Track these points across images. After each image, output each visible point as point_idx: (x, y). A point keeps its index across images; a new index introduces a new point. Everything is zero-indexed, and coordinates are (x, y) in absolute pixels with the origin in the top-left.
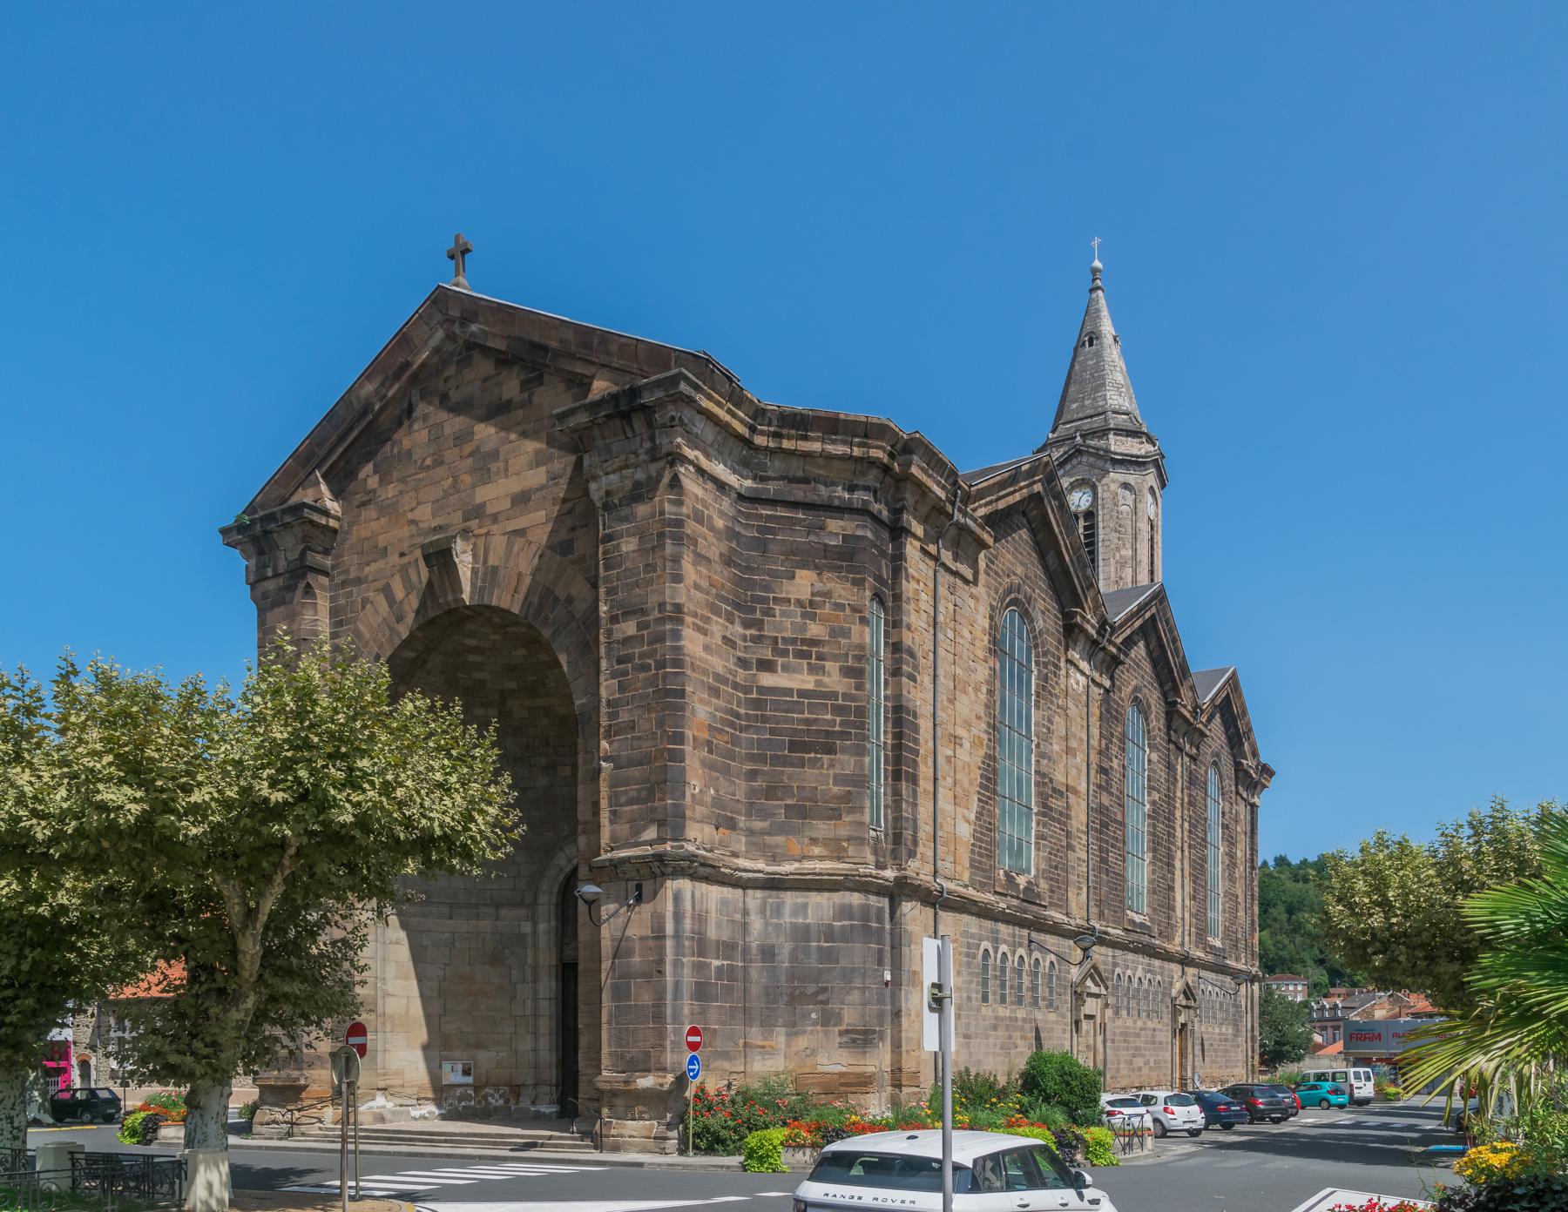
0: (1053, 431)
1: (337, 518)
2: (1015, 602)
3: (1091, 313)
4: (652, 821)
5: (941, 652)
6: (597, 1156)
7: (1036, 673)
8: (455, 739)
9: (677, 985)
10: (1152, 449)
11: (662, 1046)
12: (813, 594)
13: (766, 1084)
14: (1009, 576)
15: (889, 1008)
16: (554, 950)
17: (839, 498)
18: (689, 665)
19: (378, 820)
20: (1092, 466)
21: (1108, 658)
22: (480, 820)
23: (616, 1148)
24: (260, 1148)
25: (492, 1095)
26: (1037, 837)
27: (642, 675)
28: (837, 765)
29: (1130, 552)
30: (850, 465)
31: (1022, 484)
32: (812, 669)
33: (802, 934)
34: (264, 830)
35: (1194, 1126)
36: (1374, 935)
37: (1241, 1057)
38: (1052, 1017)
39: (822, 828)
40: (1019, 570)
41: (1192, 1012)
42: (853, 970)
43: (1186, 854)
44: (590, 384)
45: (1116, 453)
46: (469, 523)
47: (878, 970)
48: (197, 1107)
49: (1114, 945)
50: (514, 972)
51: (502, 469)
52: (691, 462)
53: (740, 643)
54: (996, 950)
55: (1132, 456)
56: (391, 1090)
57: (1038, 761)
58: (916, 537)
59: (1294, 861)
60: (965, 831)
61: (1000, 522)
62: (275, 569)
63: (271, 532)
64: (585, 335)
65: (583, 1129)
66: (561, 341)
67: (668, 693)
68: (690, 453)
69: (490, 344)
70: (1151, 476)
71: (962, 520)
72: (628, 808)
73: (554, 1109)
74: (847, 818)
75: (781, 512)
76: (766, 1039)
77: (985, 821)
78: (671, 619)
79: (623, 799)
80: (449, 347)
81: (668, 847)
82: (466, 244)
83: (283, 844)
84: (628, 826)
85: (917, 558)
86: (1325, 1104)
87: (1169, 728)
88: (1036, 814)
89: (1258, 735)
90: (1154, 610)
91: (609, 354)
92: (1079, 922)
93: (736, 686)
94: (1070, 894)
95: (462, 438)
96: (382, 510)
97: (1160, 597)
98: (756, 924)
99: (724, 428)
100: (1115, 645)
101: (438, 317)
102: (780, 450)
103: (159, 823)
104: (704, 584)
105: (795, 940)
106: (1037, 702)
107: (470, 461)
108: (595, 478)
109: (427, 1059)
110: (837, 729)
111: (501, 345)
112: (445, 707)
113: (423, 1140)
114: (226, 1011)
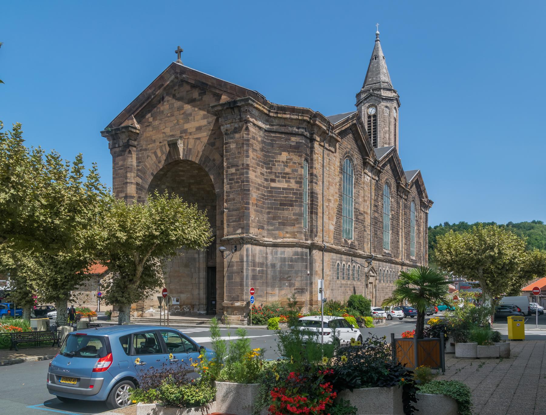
1: (139, 130)
2: (348, 156)
3: (376, 49)
4: (240, 227)
5: (325, 174)
6: (225, 326)
7: (354, 177)
9: (247, 275)
10: (395, 94)
11: (243, 294)
12: (287, 159)
13: (273, 305)
15: (309, 282)
16: (205, 263)
17: (295, 131)
20: (375, 100)
22: (203, 236)
23: (228, 324)
25: (185, 308)
26: (354, 228)
27: (237, 185)
29: (388, 129)
30: (298, 121)
32: (287, 182)
33: (283, 260)
35: (401, 317)
38: (359, 283)
39: (289, 229)
40: (349, 147)
42: (298, 270)
43: (403, 230)
46: (182, 135)
48: (123, 311)
49: (379, 260)
50: (192, 270)
52: (252, 122)
53: (265, 174)
54: (341, 263)
56: (154, 306)
58: (317, 141)
59: (451, 224)
60: (332, 228)
61: (343, 134)
62: (119, 145)
63: (118, 134)
64: (220, 83)
66: (212, 83)
67: (245, 190)
68: (251, 120)
70: (395, 104)
71: (331, 135)
72: (232, 223)
73: (205, 312)
74: (297, 226)
75: (278, 135)
78: (246, 168)
79: (231, 221)
80: (176, 80)
81: (245, 235)
84: (232, 229)
87: (398, 191)
89: (428, 191)
92: (368, 254)
93: (264, 187)
95: (180, 108)
96: (154, 128)
97: (394, 150)
98: (270, 257)
101: (173, 71)
102: (278, 117)
103: (130, 241)
104: (255, 157)
106: (355, 186)
107: (182, 116)
108: (222, 125)
110: (294, 199)
111: (193, 82)
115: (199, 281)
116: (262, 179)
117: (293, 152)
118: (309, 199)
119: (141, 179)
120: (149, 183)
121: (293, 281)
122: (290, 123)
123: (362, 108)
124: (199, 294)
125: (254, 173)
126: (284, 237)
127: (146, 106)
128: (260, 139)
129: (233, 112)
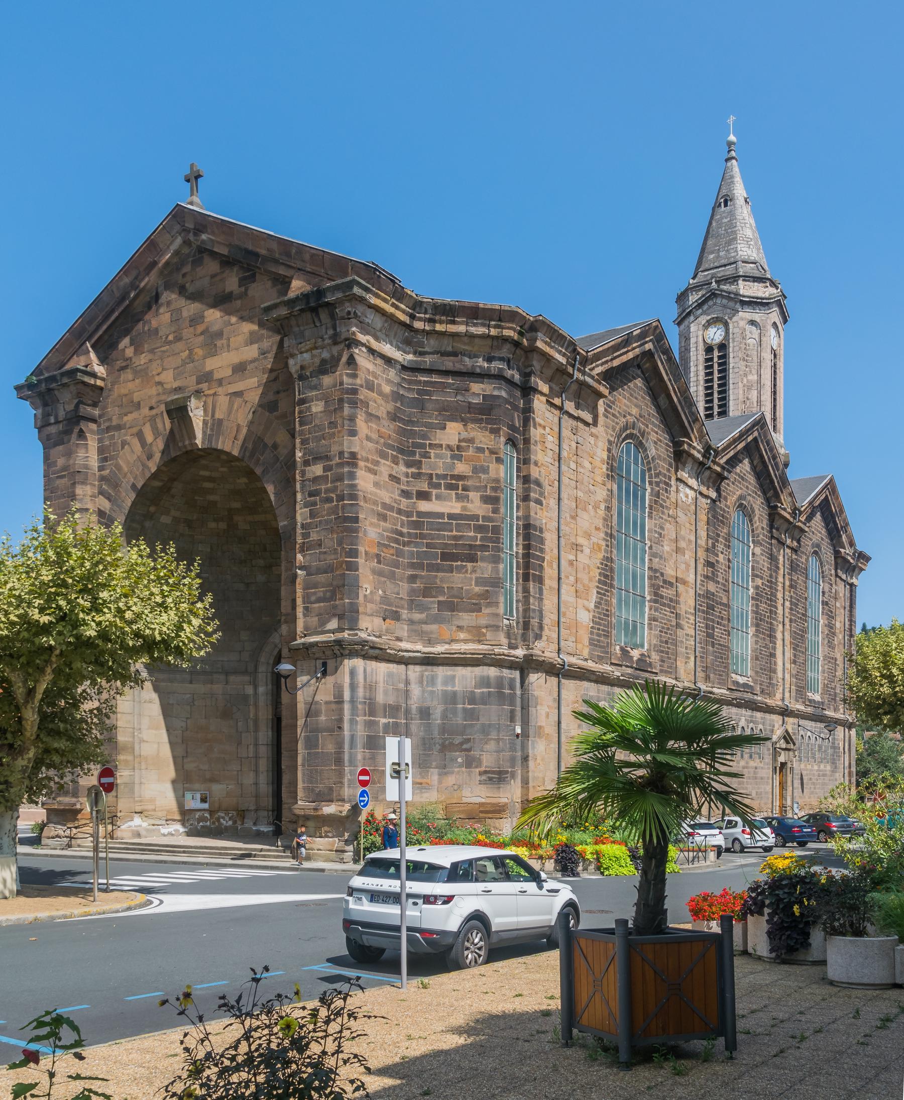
0: (694, 278)
1: (103, 379)
3: (726, 179)
4: (334, 615)
5: (565, 480)
7: (649, 490)
8: (171, 571)
9: (352, 737)
10: (775, 291)
11: (341, 783)
12: (460, 441)
14: (625, 416)
15: (519, 754)
17: (480, 367)
18: (362, 498)
19: (115, 634)
20: (724, 306)
21: (714, 475)
22: (188, 630)
24: (46, 855)
25: (223, 818)
26: (650, 619)
27: (327, 506)
28: (478, 571)
29: (755, 377)
30: (489, 342)
31: (634, 345)
32: (459, 498)
33: (451, 698)
34: (37, 640)
35: (766, 844)
36: (884, 700)
39: (466, 619)
40: (634, 411)
41: (791, 753)
42: (490, 725)
43: (787, 627)
44: (290, 283)
45: (744, 296)
46: (200, 386)
47: (510, 726)
50: (240, 724)
51: (225, 345)
52: (363, 345)
53: (404, 479)
55: (757, 298)
56: (145, 813)
57: (651, 560)
60: (585, 618)
62: (56, 417)
63: (53, 390)
65: (285, 844)
66: (268, 250)
67: (346, 519)
69: (215, 250)
71: (581, 378)
74: (486, 611)
75: (435, 378)
76: (423, 778)
77: (603, 609)
78: (348, 463)
79: (313, 598)
80: (186, 250)
81: (346, 634)
82: (198, 171)
83: (51, 648)
84: (316, 619)
85: (544, 409)
87: (771, 526)
88: (650, 601)
89: (854, 528)
90: (756, 434)
91: (303, 261)
92: (687, 684)
93: (400, 512)
94: (678, 663)
96: (137, 373)
98: (416, 691)
99: (391, 318)
100: (719, 465)
101: (177, 227)
104: (374, 436)
105: (446, 703)
106: (650, 513)
107: (202, 338)
108: (292, 356)
109: (175, 790)
110: (478, 543)
111: (224, 251)
112: (164, 550)
113: (168, 851)
114: (14, 759)
115: (256, 752)
116: (393, 493)
117: (475, 421)
118: (521, 542)
119: (110, 500)
120: (127, 509)
121: (475, 753)
122: (466, 347)
124: (256, 784)
125: (372, 476)
126: (452, 641)
127: (117, 318)
128: (387, 389)
129: (316, 320)
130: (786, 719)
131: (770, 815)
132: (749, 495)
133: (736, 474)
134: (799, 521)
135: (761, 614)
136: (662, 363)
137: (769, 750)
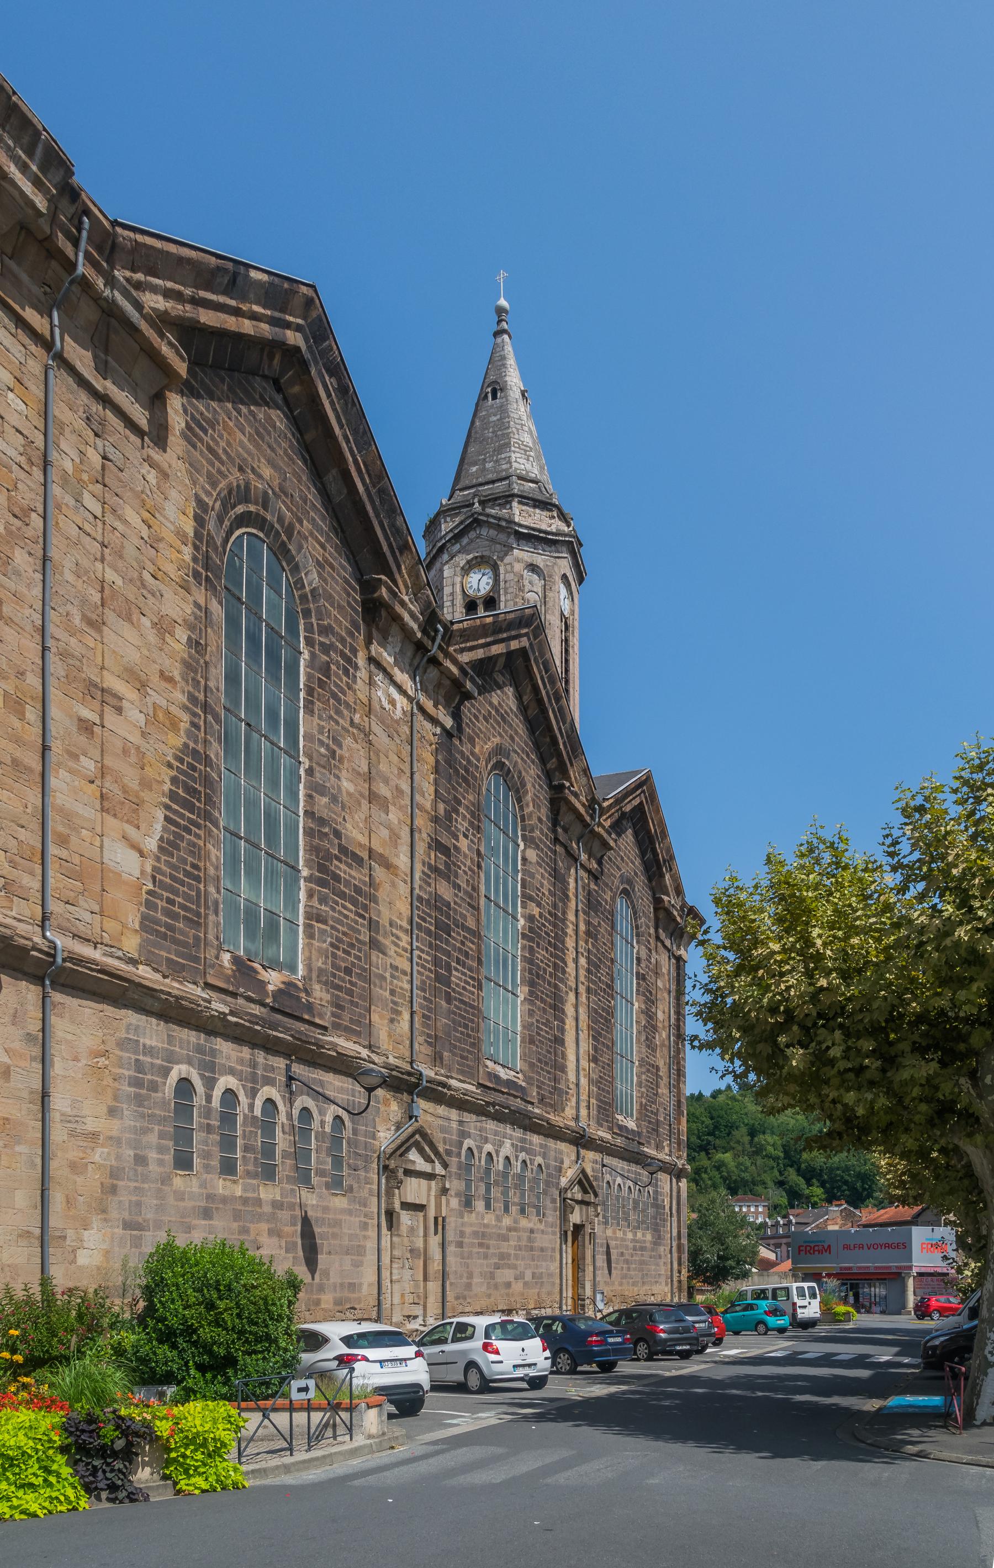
3: (496, 361)
7: (306, 655)
10: (566, 529)
20: (493, 540)
26: (308, 916)
35: (532, 1373)
36: (789, 1013)
37: (664, 1270)
38: (340, 1202)
41: (591, 1209)
43: (583, 998)
49: (461, 1104)
54: (210, 1083)
55: (540, 531)
57: (309, 797)
86: (761, 1328)
87: (555, 822)
88: (306, 879)
94: (375, 1018)
100: (455, 662)
123: (446, 574)
130: (583, 1152)
131: (557, 1312)
132: (516, 752)
133: (491, 704)
134: (600, 824)
135: (539, 967)
136: (329, 396)
137: (554, 1201)
